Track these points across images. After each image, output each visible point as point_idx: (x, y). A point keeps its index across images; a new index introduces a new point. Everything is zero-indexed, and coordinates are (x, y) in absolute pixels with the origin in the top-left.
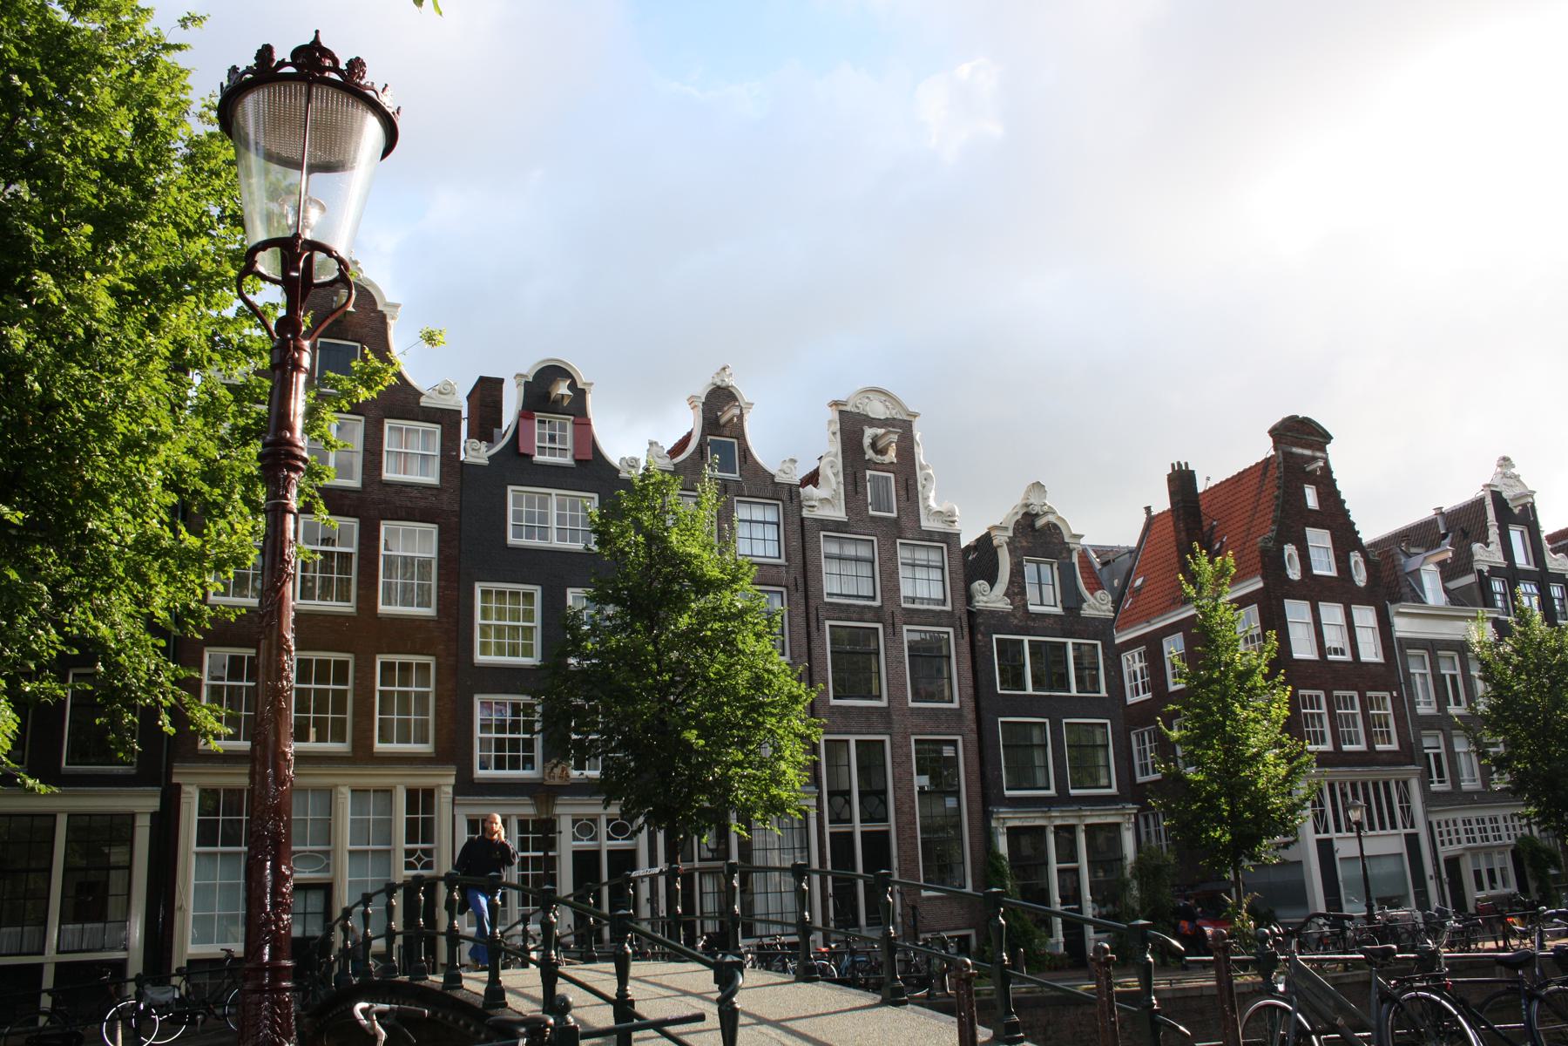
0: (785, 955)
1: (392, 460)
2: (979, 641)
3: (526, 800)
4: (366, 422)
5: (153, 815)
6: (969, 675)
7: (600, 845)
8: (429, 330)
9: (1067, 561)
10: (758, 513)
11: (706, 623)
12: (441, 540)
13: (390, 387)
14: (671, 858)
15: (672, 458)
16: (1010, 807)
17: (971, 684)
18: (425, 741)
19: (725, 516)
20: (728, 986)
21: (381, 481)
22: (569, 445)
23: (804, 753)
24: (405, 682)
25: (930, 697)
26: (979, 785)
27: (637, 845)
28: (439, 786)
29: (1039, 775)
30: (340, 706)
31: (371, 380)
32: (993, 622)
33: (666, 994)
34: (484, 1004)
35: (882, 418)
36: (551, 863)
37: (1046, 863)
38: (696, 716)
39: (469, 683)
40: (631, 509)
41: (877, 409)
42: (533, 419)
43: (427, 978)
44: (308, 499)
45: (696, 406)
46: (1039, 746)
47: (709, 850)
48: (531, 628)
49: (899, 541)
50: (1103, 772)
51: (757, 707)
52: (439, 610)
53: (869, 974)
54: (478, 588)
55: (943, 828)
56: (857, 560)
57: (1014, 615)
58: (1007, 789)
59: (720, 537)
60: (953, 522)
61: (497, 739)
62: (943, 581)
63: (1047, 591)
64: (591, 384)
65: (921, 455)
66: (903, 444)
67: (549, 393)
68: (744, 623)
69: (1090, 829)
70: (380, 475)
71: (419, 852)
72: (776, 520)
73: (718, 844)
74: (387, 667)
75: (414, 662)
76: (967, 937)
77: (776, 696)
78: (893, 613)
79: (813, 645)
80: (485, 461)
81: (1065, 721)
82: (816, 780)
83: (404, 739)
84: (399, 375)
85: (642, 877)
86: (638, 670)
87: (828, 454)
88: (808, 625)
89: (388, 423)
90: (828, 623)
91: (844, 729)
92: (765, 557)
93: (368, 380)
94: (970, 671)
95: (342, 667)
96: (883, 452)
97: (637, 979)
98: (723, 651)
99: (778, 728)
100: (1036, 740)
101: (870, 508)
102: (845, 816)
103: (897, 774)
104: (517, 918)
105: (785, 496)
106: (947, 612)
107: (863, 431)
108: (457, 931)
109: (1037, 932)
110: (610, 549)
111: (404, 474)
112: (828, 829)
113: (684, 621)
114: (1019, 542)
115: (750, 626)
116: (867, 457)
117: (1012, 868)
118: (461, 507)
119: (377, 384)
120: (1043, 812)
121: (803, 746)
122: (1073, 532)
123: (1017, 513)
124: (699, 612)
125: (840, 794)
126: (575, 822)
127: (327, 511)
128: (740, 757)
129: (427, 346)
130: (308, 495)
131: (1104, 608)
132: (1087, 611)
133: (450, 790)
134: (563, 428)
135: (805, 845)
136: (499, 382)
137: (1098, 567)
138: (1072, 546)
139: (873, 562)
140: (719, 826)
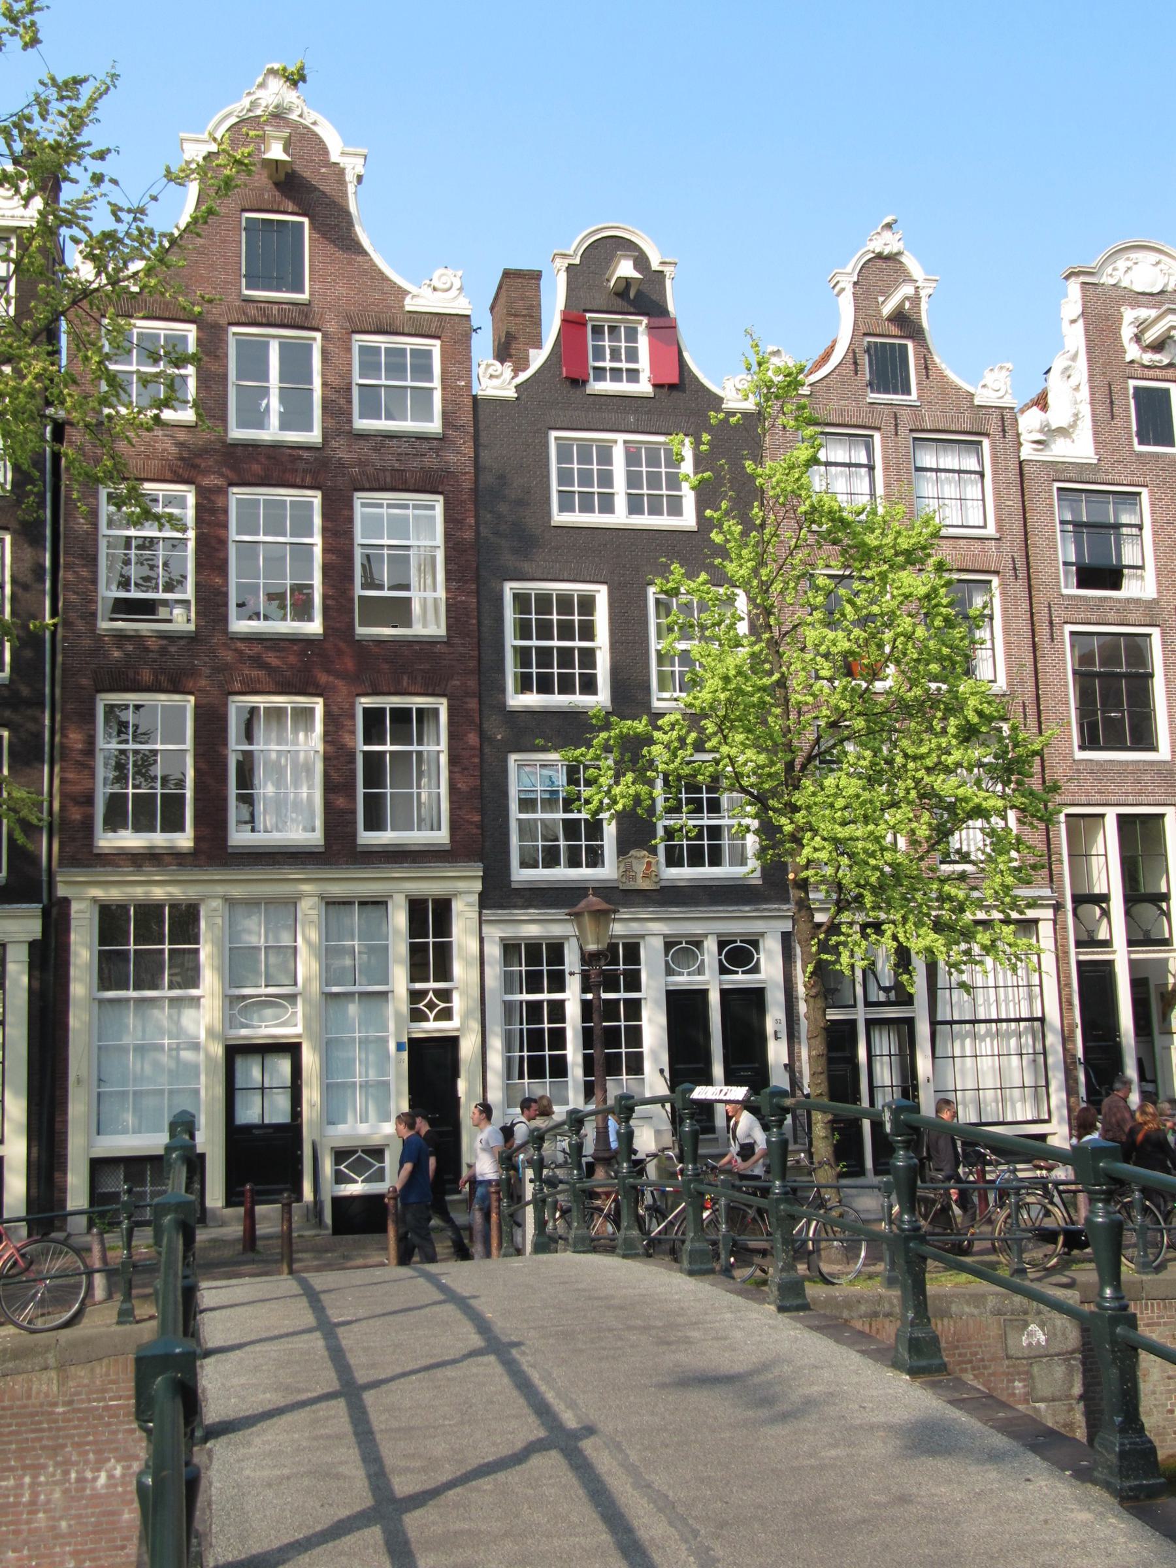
5: (32, 945)
12: (448, 519)
22: (644, 363)
47: (881, 988)
75: (388, 707)
80: (511, 393)
102: (1102, 935)
126: (721, 945)
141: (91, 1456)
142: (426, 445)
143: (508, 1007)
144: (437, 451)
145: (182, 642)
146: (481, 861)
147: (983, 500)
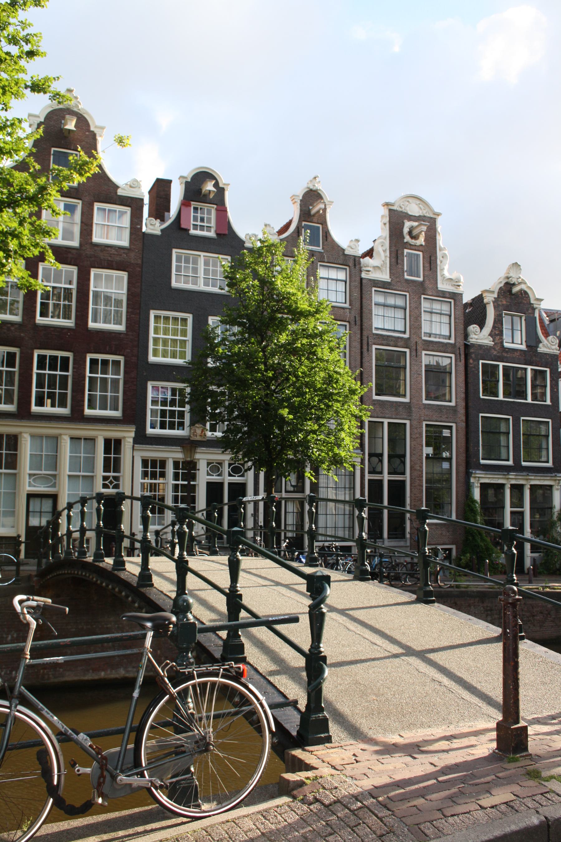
0: (338, 555)
1: (99, 228)
2: (471, 364)
3: (179, 449)
4: (83, 204)
6: (462, 385)
7: (224, 479)
8: (120, 136)
9: (532, 315)
10: (333, 274)
11: (298, 339)
12: (129, 283)
13: (94, 175)
14: (268, 490)
15: (279, 235)
16: (484, 471)
17: (464, 391)
18: (116, 409)
19: (311, 272)
20: (319, 595)
21: (91, 243)
22: (213, 224)
23: (356, 427)
24: (104, 372)
25: (436, 399)
26: (464, 455)
27: (246, 480)
28: (124, 438)
29: (503, 451)
30: (64, 385)
31: (82, 169)
32: (480, 352)
33: (264, 584)
34: (138, 583)
35: (417, 215)
36: (193, 488)
37: (503, 507)
38: (288, 399)
39: (145, 374)
40: (251, 263)
41: (414, 209)
42: (190, 206)
43: (104, 561)
44: (41, 250)
45: (295, 202)
46: (504, 433)
47: (291, 485)
48: (185, 341)
49: (423, 296)
50: (544, 453)
51: (329, 396)
52: (127, 327)
53: (390, 570)
54: (152, 314)
55: (439, 481)
56: (395, 307)
57: (494, 349)
58: (483, 459)
59: (308, 284)
60: (459, 286)
61: (162, 410)
62: (450, 324)
63: (517, 335)
64: (228, 185)
65: (441, 241)
66: (430, 233)
67: (201, 190)
68: (323, 341)
69: (533, 488)
70: (91, 239)
71: (111, 478)
72: (344, 279)
73: (298, 482)
74: (94, 362)
76: (450, 550)
77: (341, 389)
78: (416, 342)
79: (364, 360)
80: (158, 233)
81: (522, 418)
82: (362, 445)
83: (104, 407)
84: (100, 167)
85: (249, 502)
86: (251, 367)
87: (380, 238)
88: (362, 348)
89: (96, 205)
90: (374, 347)
91: (381, 415)
92: (336, 302)
93: (81, 168)
94: (464, 382)
95: (65, 360)
96: (415, 238)
97: (244, 570)
98: (308, 358)
99: (341, 410)
100: (503, 429)
101: (405, 274)
102: (379, 469)
103: (412, 445)
104: (170, 522)
105: (351, 264)
106: (451, 344)
107: (403, 223)
108: (123, 532)
109: (495, 549)
110: (236, 289)
111: (107, 238)
112: (367, 477)
113: (283, 338)
114: (501, 301)
115: (326, 342)
116: (405, 241)
117: (482, 508)
118: (142, 262)
119: (86, 172)
120: (504, 475)
121: (357, 423)
122: (537, 297)
123: (501, 282)
124: (293, 332)
125: (376, 456)
126: (208, 464)
127: (54, 257)
128: (316, 427)
129: (119, 147)
130: (42, 247)
131: (553, 347)
132: (542, 349)
133: (131, 440)
134: (209, 213)
135: (352, 486)
136: (168, 183)
137: (547, 322)
138: (535, 306)
139: (405, 309)
140: (298, 472)
141: (6, 630)
142: (122, 251)
143: (143, 485)
144: (126, 254)
145: (16, 326)
146: (135, 424)
147: (345, 292)
